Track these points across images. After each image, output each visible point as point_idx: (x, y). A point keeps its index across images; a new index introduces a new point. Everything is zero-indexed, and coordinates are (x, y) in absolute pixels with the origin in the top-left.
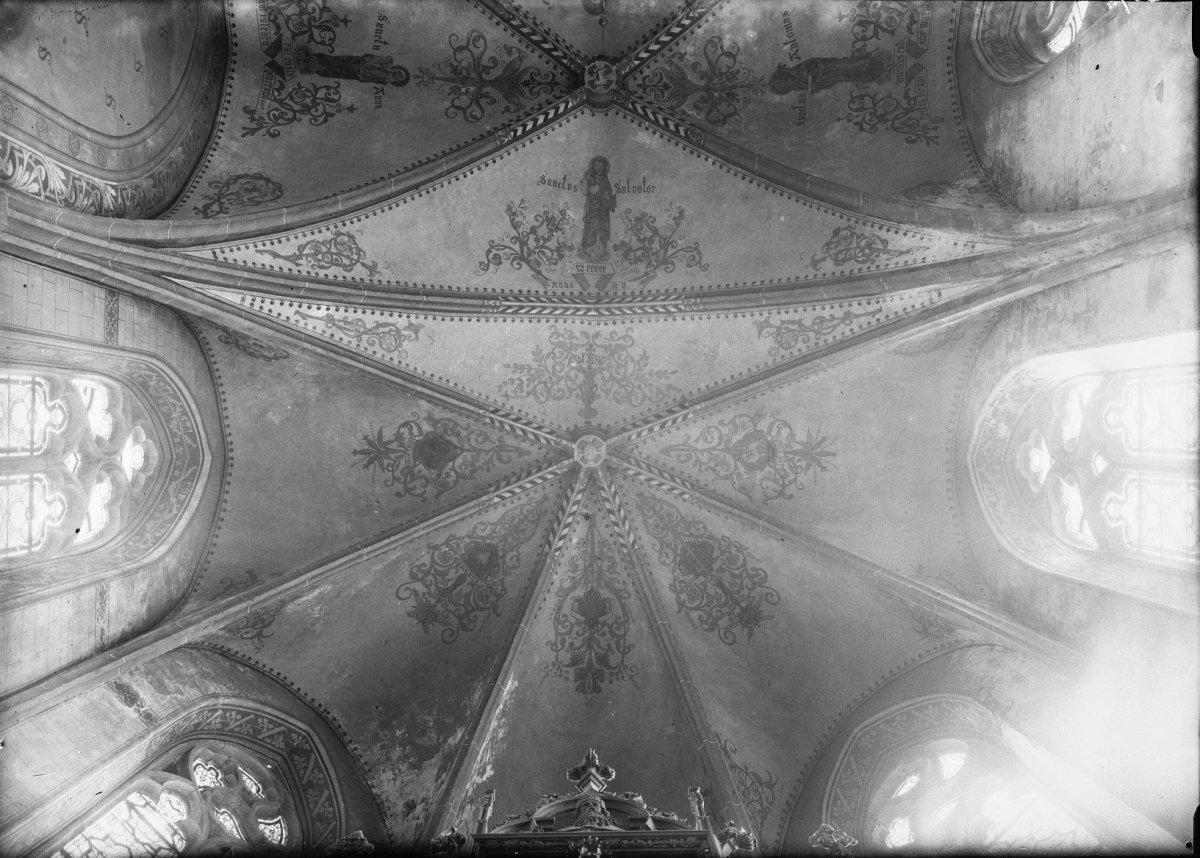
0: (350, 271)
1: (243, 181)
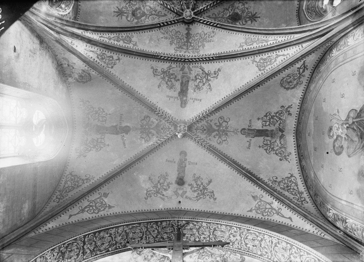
0: (261, 58)
1: (292, 86)
